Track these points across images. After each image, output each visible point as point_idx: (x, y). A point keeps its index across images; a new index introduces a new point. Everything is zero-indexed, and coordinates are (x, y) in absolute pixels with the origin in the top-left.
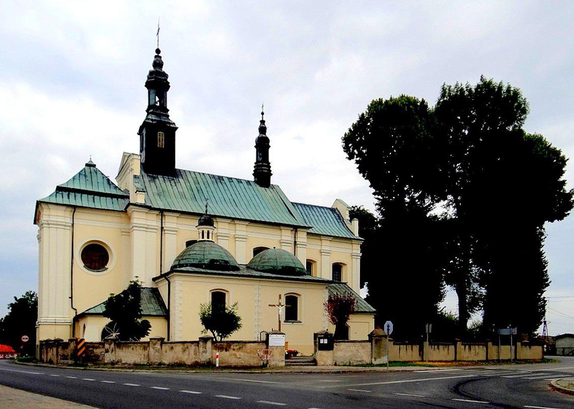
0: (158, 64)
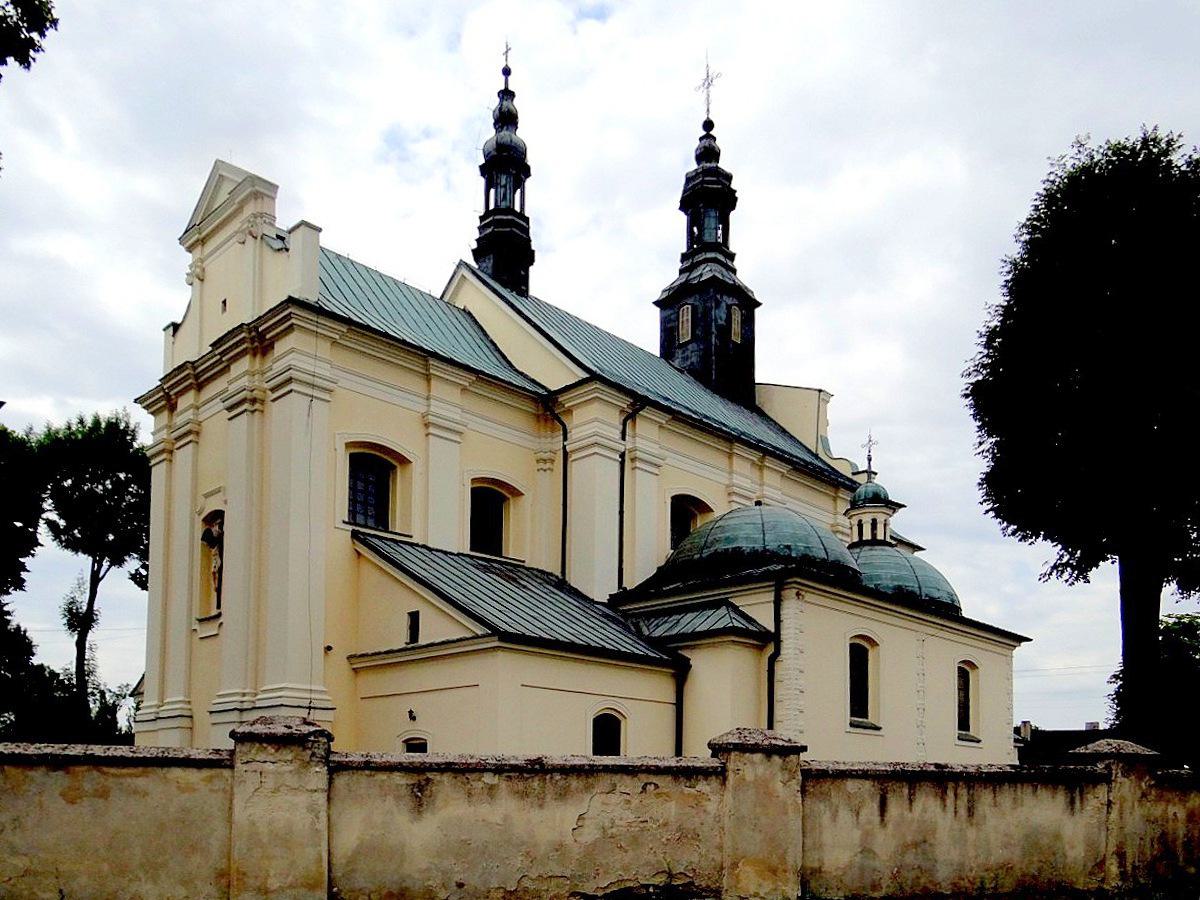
0: (708, 153)
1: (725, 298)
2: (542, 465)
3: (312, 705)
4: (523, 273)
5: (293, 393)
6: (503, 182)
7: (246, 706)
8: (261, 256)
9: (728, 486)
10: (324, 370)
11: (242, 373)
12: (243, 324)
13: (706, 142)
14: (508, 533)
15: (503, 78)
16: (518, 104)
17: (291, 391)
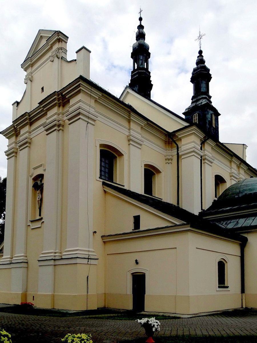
0: (201, 61)
1: (210, 111)
2: (167, 161)
3: (90, 257)
4: (149, 93)
5: (80, 119)
6: (141, 58)
7: (57, 258)
8: (61, 66)
9: (230, 173)
10: (92, 111)
11: (53, 113)
12: (55, 92)
13: (200, 58)
14: (155, 186)
16: (145, 30)
17: (80, 118)
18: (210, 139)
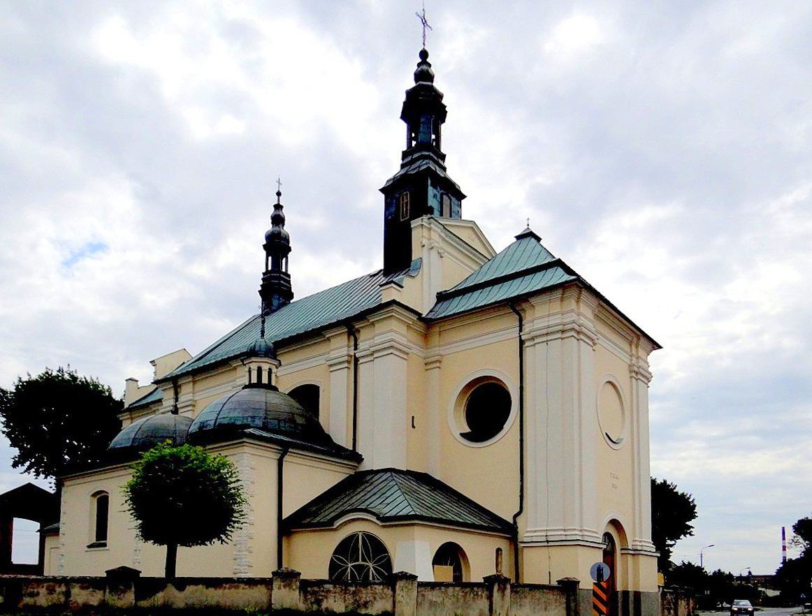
0: (424, 75)
15: (277, 197)
16: (285, 212)
18: (290, 450)
